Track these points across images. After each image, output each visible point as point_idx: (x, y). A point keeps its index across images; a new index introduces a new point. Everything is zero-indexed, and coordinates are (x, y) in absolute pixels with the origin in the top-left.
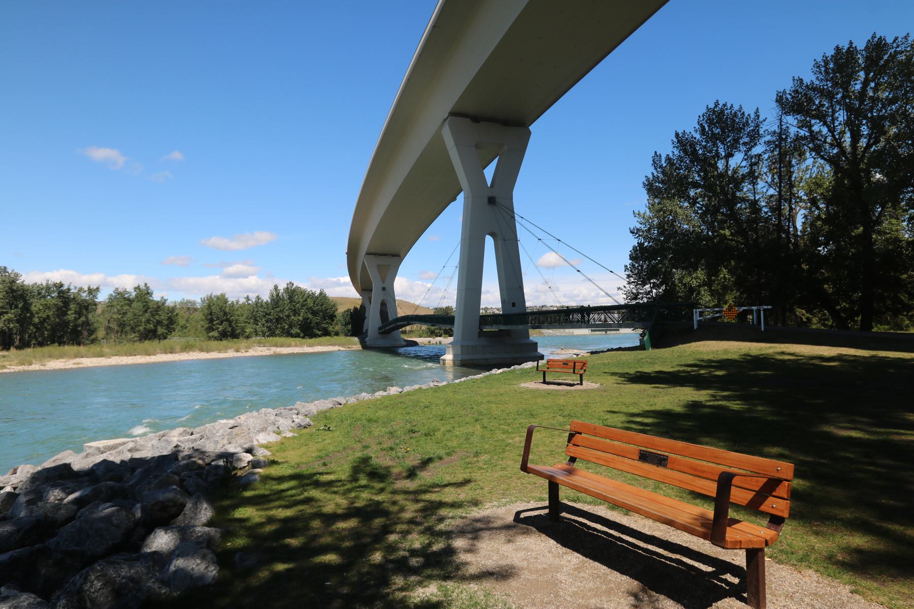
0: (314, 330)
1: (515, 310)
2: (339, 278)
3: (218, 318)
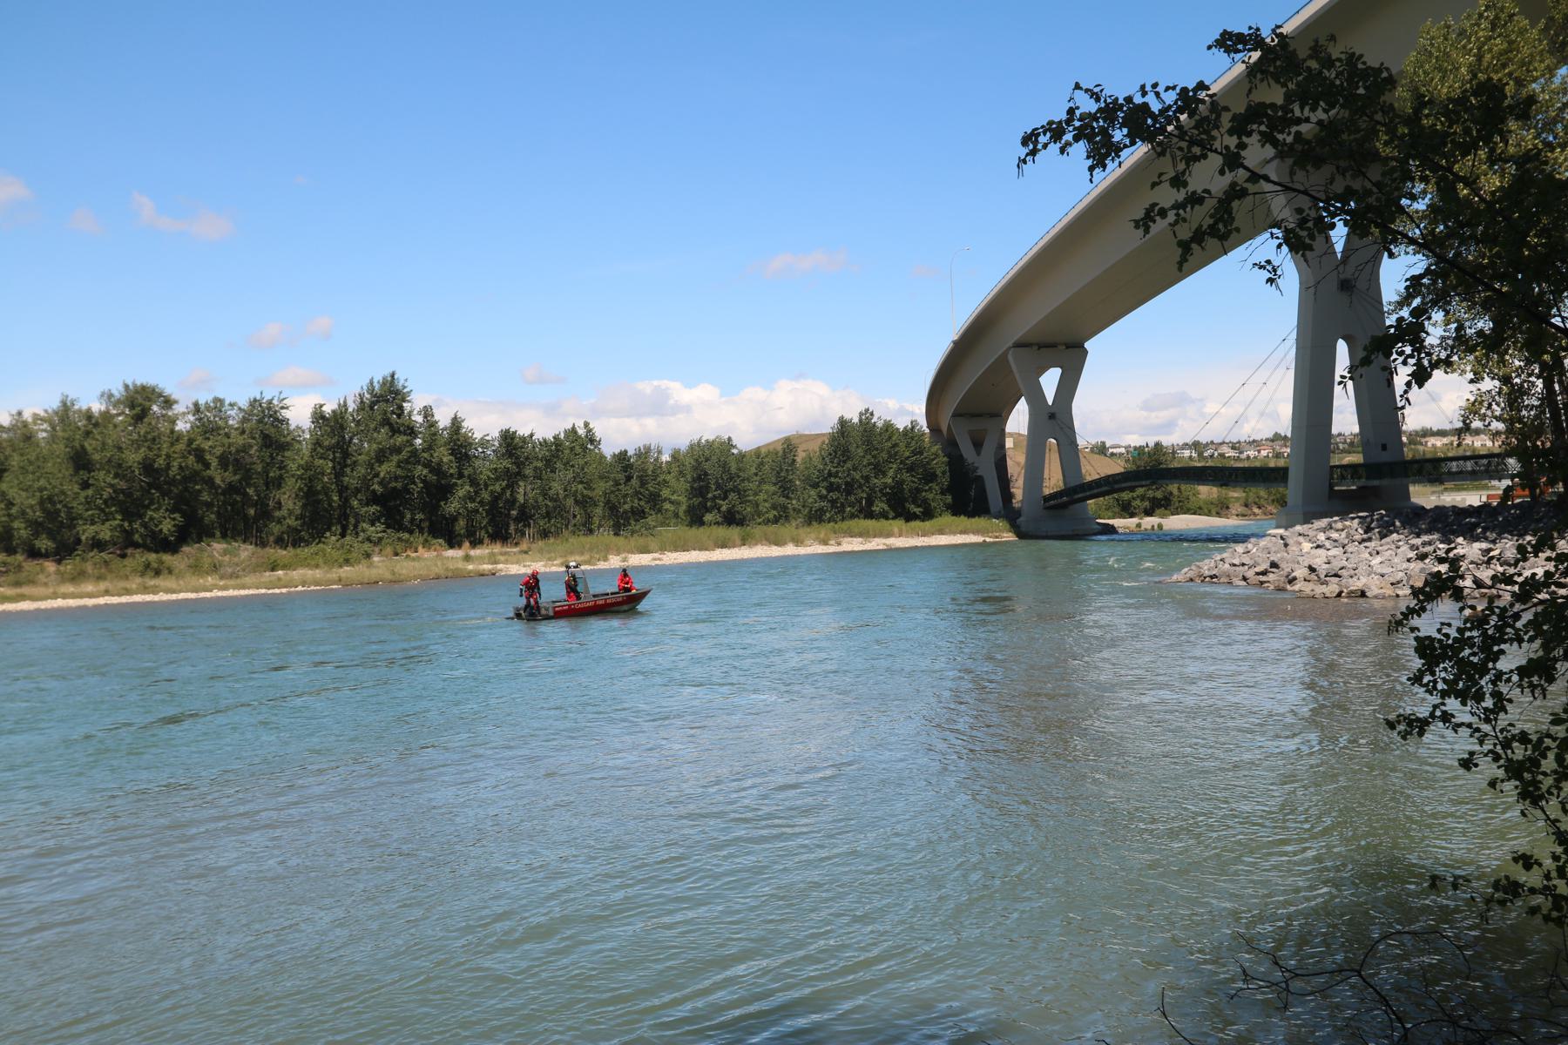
0: (907, 505)
1: (1385, 457)
3: (718, 487)
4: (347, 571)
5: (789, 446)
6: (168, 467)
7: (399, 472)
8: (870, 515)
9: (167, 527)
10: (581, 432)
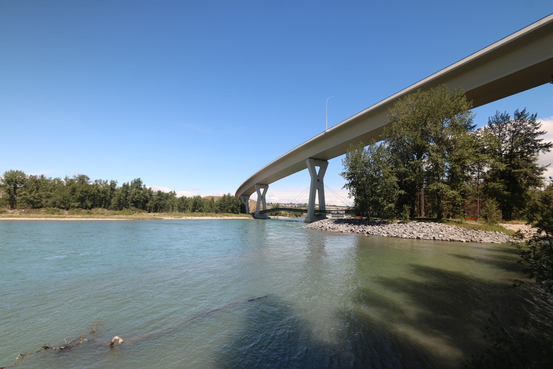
1: (323, 209)
3: (199, 205)
4: (130, 216)
5: (213, 198)
6: (91, 192)
7: (138, 197)
8: (228, 212)
9: (90, 204)
10: (173, 192)
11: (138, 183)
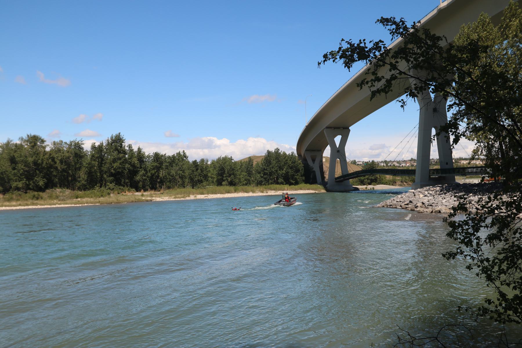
2: (212, 138)
4: (102, 199)
6: (42, 163)
8: (278, 183)
9: (41, 183)
10: (182, 154)
11: (117, 141)
